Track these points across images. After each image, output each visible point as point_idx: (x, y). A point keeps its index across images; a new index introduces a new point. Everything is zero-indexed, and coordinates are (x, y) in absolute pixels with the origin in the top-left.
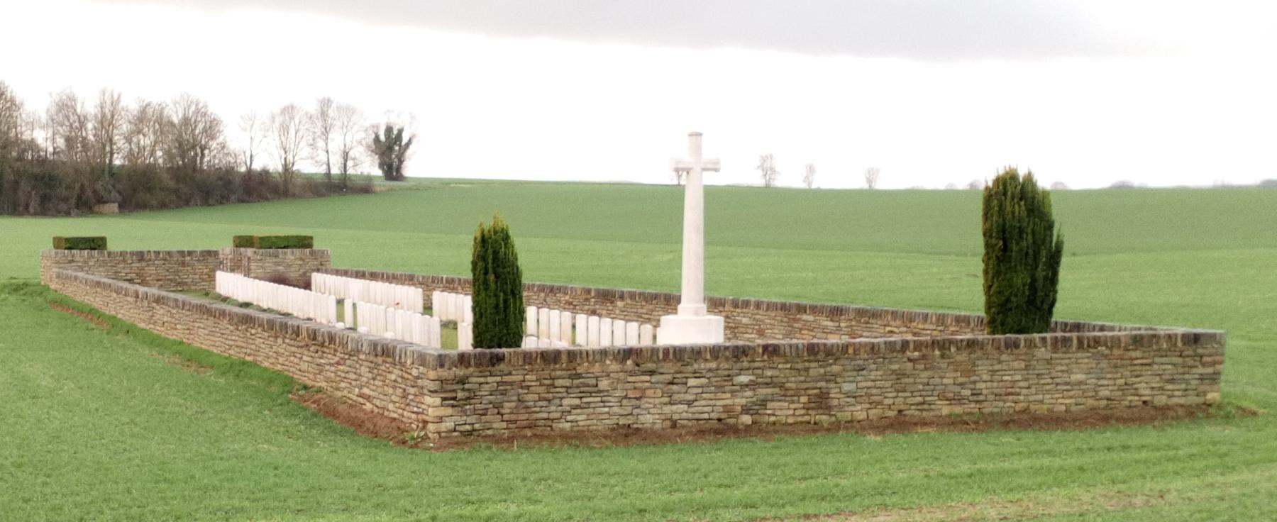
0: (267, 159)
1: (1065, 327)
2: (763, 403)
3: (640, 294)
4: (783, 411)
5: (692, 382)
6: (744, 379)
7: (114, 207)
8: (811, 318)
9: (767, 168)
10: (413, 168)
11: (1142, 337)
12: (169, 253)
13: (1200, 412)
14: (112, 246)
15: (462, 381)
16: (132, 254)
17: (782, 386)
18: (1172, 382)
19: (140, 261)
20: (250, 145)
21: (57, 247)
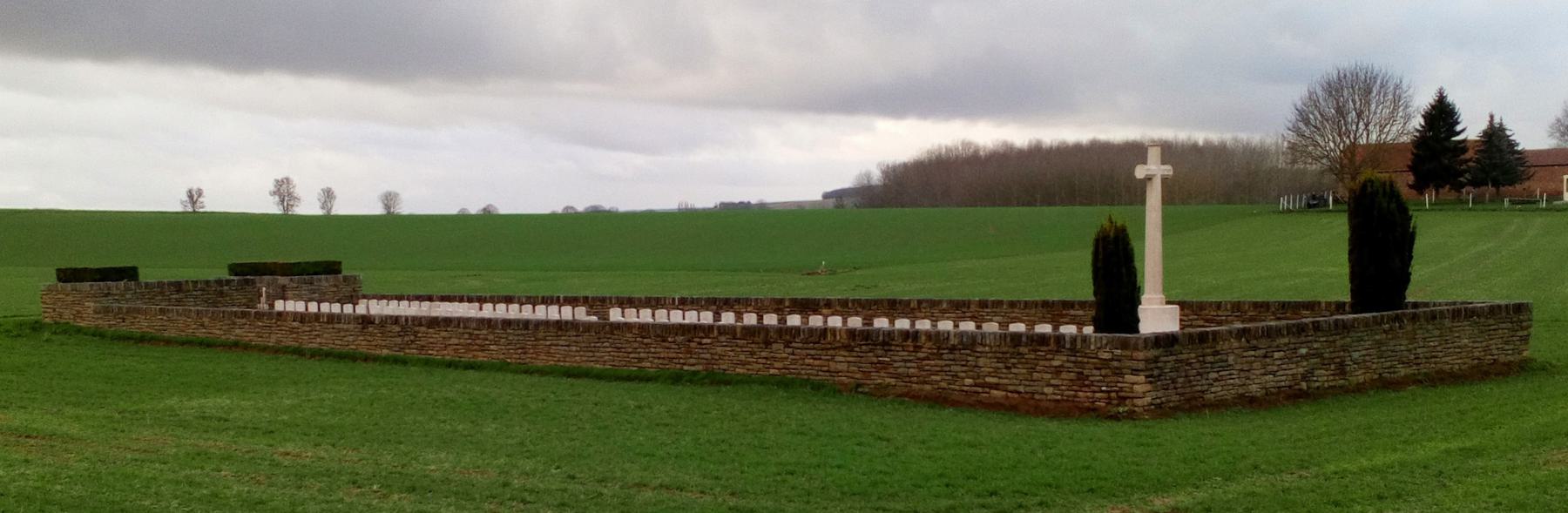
1: (1415, 305)
2: (1311, 372)
3: (854, 301)
5: (1277, 355)
6: (1304, 351)
8: (1081, 312)
9: (283, 190)
11: (1459, 311)
12: (207, 282)
14: (147, 275)
15: (1156, 360)
16: (170, 284)
17: (1320, 356)
18: (1494, 344)
19: (178, 291)
21: (60, 280)
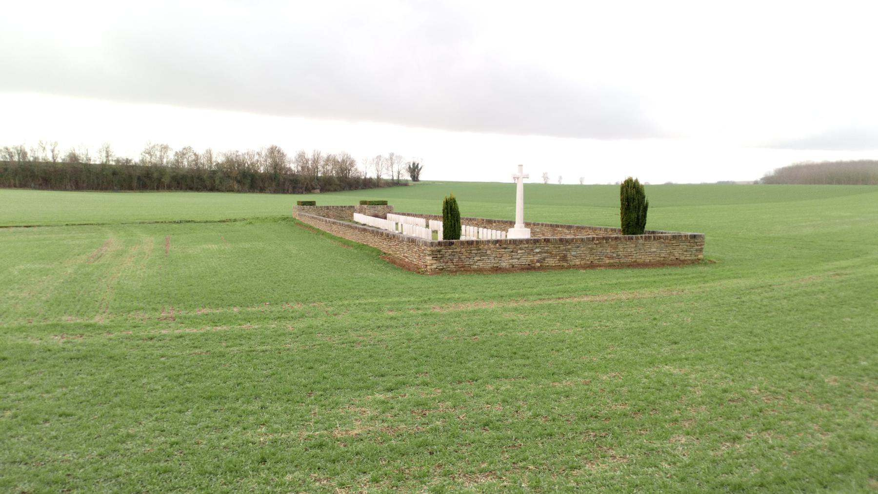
0: (372, 174)
4: (551, 262)
7: (318, 191)
9: (545, 177)
10: (422, 177)
13: (696, 262)
20: (365, 169)
